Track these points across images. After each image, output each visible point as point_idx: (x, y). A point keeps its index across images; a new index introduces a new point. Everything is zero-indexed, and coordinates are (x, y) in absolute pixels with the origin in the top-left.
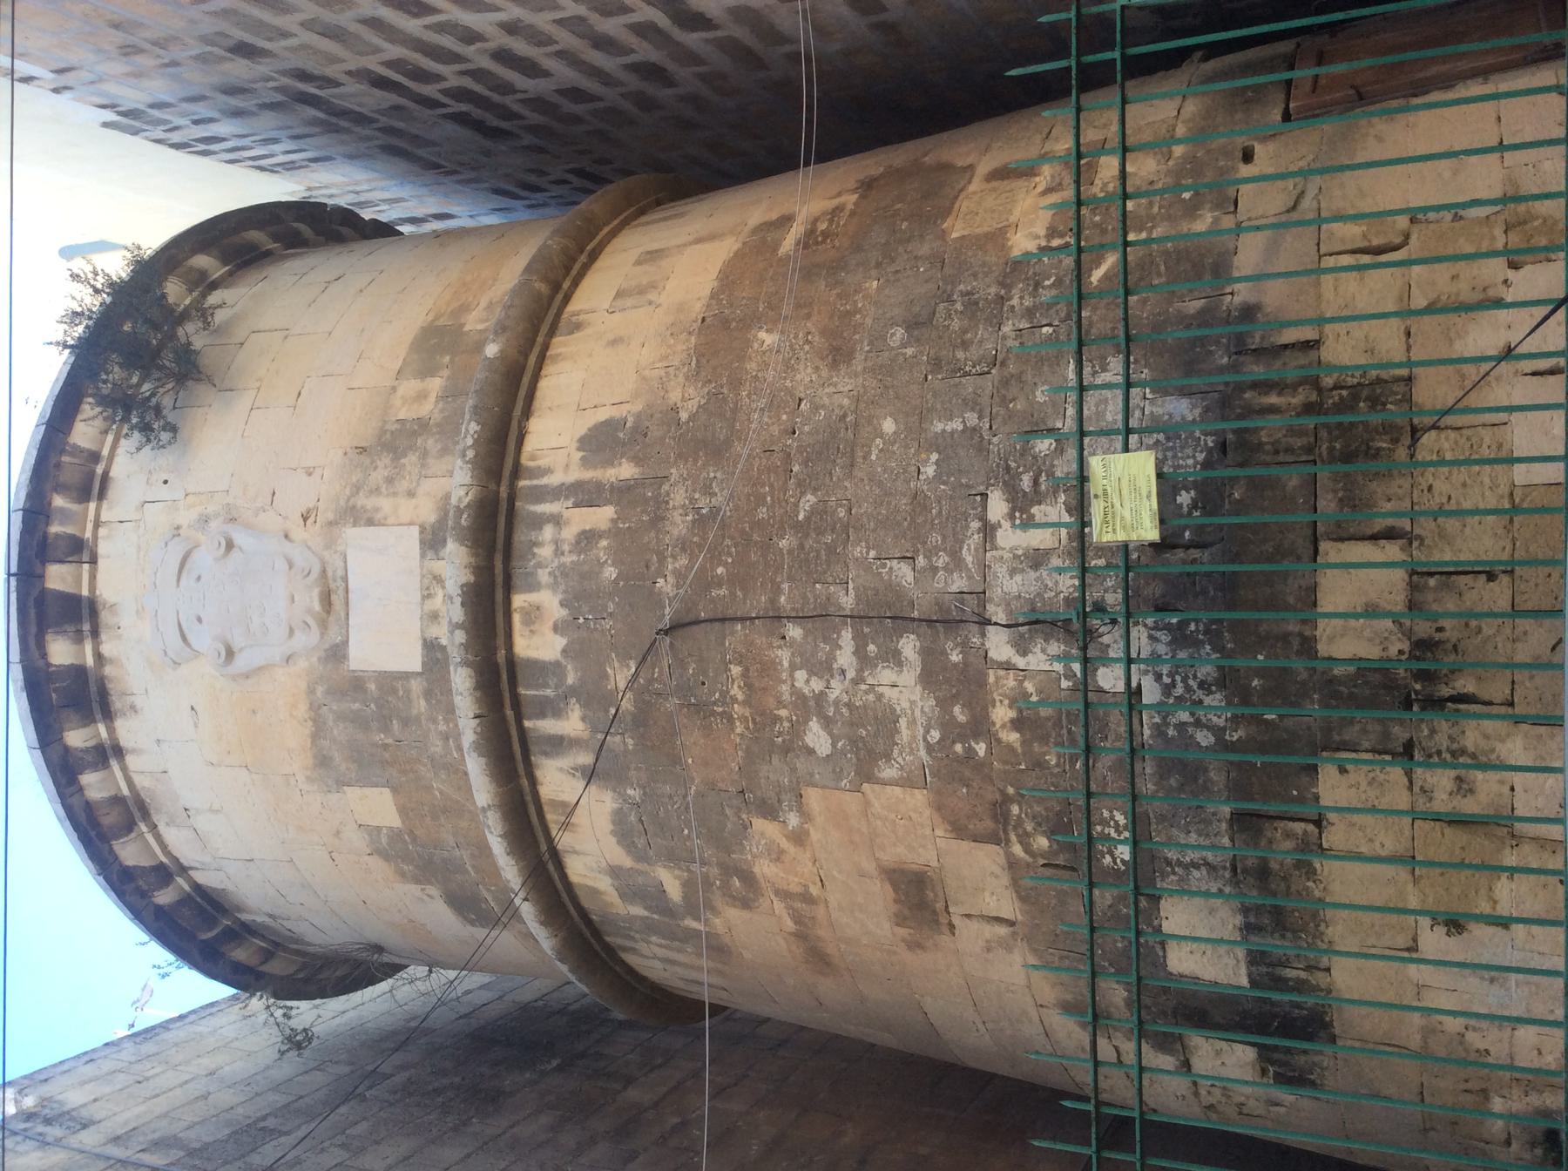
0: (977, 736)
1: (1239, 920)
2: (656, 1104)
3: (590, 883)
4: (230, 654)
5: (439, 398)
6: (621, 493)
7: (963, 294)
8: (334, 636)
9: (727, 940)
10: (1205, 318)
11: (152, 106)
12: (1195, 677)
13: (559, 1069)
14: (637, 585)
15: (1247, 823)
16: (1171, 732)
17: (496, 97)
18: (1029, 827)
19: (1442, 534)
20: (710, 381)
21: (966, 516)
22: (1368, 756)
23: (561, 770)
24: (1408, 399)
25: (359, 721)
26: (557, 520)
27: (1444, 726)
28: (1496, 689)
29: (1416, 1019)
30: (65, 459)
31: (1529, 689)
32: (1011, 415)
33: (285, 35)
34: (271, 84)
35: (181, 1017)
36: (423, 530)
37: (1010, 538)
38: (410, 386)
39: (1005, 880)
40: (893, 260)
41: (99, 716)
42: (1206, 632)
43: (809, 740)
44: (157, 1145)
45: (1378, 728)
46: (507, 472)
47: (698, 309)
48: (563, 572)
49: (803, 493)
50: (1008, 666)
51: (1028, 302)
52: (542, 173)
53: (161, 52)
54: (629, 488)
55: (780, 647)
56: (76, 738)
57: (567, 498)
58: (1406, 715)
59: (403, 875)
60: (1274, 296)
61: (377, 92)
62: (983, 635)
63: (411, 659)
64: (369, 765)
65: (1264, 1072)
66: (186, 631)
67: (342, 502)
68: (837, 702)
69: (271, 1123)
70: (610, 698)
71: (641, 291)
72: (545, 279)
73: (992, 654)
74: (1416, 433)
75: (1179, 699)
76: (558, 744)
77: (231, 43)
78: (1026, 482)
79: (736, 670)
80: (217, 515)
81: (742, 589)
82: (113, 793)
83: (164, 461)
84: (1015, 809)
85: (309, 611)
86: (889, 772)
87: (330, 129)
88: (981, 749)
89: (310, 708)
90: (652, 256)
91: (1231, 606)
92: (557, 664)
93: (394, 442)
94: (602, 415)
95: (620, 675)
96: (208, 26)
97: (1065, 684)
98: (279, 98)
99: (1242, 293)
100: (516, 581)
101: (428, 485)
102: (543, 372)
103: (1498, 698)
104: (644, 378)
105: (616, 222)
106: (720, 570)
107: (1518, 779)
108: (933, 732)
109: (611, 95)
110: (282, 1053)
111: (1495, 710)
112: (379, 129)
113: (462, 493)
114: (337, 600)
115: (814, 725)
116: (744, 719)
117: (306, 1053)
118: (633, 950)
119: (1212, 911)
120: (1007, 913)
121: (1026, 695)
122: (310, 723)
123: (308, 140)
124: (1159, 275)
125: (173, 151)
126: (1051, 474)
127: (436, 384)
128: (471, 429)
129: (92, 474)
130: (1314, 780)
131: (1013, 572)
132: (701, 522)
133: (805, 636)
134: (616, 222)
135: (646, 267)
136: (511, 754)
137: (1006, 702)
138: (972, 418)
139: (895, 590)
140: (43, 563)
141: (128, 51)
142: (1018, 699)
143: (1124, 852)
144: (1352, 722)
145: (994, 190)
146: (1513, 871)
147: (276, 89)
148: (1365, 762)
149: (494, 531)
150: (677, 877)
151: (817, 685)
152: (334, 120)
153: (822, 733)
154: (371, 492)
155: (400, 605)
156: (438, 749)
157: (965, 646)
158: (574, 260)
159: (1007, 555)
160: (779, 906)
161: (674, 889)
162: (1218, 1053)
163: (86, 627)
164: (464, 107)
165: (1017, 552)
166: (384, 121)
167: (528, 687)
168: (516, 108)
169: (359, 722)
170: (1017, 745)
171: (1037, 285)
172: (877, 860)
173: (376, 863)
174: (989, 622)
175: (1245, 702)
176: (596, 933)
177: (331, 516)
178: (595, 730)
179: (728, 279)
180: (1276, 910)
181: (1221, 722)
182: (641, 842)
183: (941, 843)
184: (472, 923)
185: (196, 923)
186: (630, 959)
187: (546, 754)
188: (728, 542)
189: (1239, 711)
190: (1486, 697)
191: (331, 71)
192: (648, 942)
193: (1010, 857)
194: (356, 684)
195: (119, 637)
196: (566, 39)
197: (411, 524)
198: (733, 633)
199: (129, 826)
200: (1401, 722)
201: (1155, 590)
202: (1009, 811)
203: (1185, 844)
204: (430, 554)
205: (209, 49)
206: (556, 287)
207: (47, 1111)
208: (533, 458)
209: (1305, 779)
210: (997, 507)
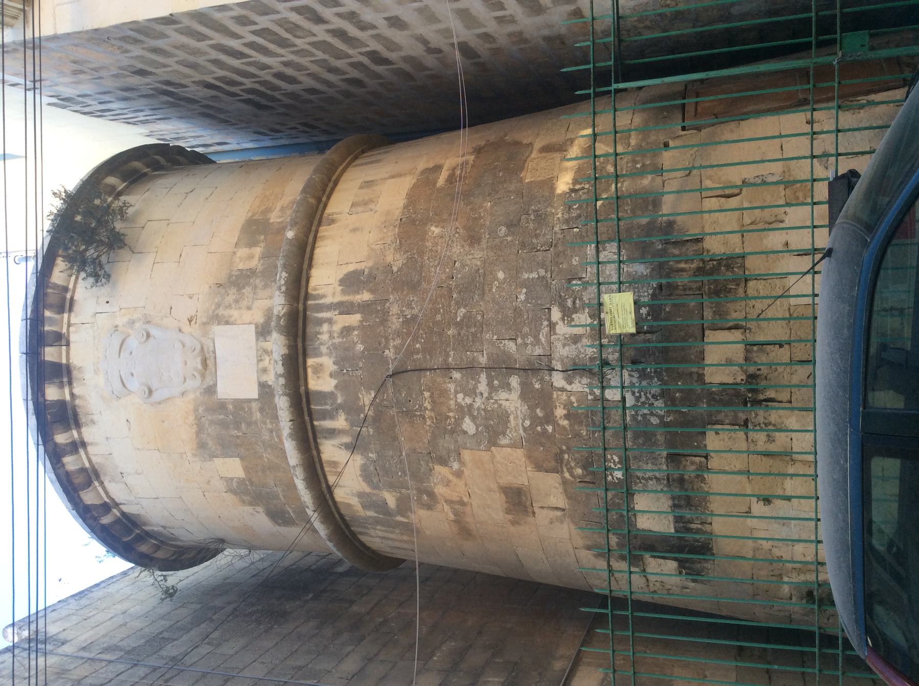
0: (548, 423)
1: (670, 503)
2: (368, 613)
3: (346, 501)
4: (151, 392)
6: (363, 308)
7: (534, 211)
8: (209, 381)
10: (650, 229)
11: (79, 96)
14: (374, 354)
15: (673, 458)
16: (639, 418)
17: (269, 92)
18: (573, 464)
19: (759, 327)
22: (728, 427)
23: (334, 445)
24: (743, 267)
25: (224, 424)
26: (330, 321)
27: (761, 413)
28: (784, 396)
29: (750, 543)
30: (49, 291)
31: (799, 396)
32: (560, 271)
35: (97, 585)
37: (562, 329)
38: (243, 252)
39: (561, 490)
40: (497, 192)
41: (73, 426)
42: (655, 372)
44: (107, 650)
45: (733, 414)
47: (397, 214)
48: (335, 347)
49: (459, 308)
50: (563, 390)
54: (368, 305)
56: (61, 438)
57: (335, 310)
58: (746, 409)
59: (243, 502)
61: (206, 90)
62: (551, 375)
63: (253, 392)
64: (227, 448)
65: (680, 573)
66: (125, 382)
67: (211, 312)
68: (478, 409)
69: (166, 635)
70: (361, 409)
71: (366, 203)
72: (314, 197)
73: (556, 384)
74: (746, 280)
75: (643, 403)
76: (332, 433)
77: (135, 69)
78: (569, 303)
79: (427, 394)
80: (139, 320)
82: (80, 466)
83: (104, 291)
84: (566, 456)
85: (196, 369)
86: (504, 441)
87: (172, 105)
88: (550, 429)
89: (196, 419)
90: (368, 184)
91: (666, 361)
92: (332, 393)
93: (237, 282)
94: (351, 268)
95: (366, 398)
96: (126, 62)
97: (590, 397)
98: (152, 92)
100: (309, 352)
101: (258, 303)
103: (785, 399)
104: (372, 249)
105: (344, 164)
106: (418, 346)
107: (794, 435)
109: (331, 92)
110: (163, 600)
111: (783, 405)
114: (210, 363)
115: (467, 420)
117: (174, 598)
118: (366, 534)
119: (658, 499)
120: (561, 505)
123: (160, 111)
124: (628, 204)
126: (581, 299)
127: (258, 251)
128: (282, 276)
129: (64, 298)
130: (705, 439)
131: (564, 346)
132: (407, 322)
133: (462, 378)
134: (347, 161)
135: (365, 191)
136: (308, 438)
138: (542, 272)
139: (508, 356)
141: (75, 73)
142: (568, 405)
143: (619, 474)
144: (721, 412)
145: (545, 158)
146: (792, 476)
147: (151, 89)
148: (728, 430)
149: (298, 327)
151: (468, 400)
153: (472, 424)
154: (227, 307)
155: (245, 363)
156: (267, 437)
157: (542, 380)
159: (561, 338)
160: (447, 508)
162: (660, 565)
163: (65, 380)
164: (250, 96)
165: (566, 337)
166: (206, 102)
167: (316, 405)
168: (279, 97)
169: (223, 425)
170: (567, 426)
171: (570, 207)
172: (498, 483)
174: (554, 370)
175: (674, 405)
176: (348, 526)
177: (205, 320)
178: (352, 425)
179: (412, 199)
180: (687, 497)
181: (662, 413)
183: (530, 474)
184: (279, 525)
185: (122, 532)
186: (363, 538)
187: (326, 438)
189: (670, 408)
190: (780, 399)
191: (183, 82)
192: (375, 529)
193: (563, 478)
194: (222, 406)
195: (84, 384)
196: (315, 68)
197: (250, 323)
199: (89, 483)
200: (743, 412)
201: (631, 353)
203: (646, 469)
204: (261, 339)
206: (319, 200)
208: (315, 289)
209: (700, 438)
210: (556, 314)
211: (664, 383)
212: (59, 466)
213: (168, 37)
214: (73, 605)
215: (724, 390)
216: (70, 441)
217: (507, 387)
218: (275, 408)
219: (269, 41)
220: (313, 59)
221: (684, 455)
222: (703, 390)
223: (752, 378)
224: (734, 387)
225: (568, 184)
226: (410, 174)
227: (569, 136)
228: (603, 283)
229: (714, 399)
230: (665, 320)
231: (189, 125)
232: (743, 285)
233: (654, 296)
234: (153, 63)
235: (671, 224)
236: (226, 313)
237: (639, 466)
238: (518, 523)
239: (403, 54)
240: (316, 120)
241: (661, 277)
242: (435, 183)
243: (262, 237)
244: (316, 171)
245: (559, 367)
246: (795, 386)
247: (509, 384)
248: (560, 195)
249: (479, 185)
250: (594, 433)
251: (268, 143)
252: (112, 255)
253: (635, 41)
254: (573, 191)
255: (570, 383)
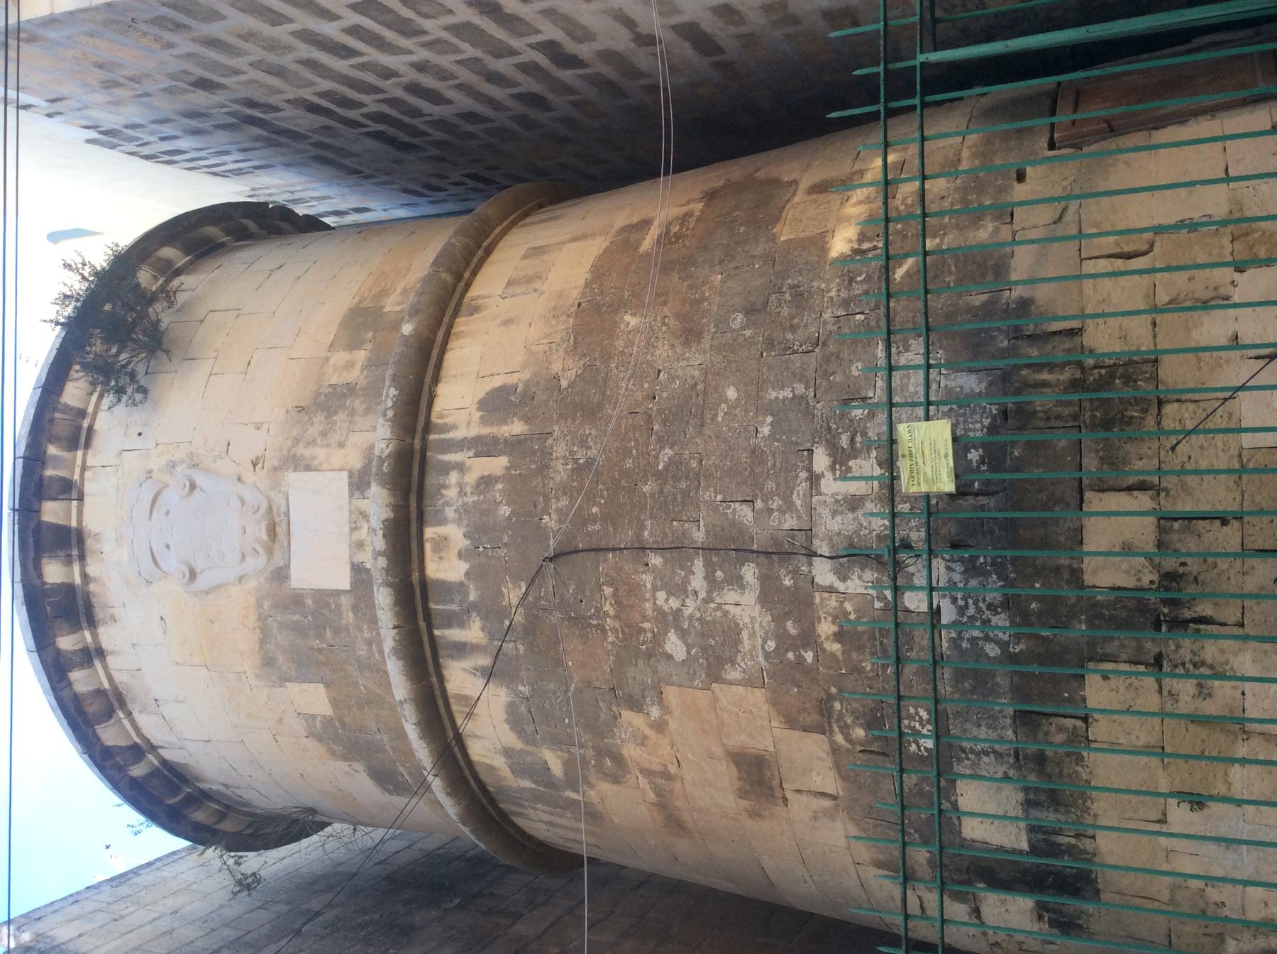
0: (805, 646)
1: (1020, 796)
3: (487, 761)
4: (193, 574)
5: (364, 367)
6: (513, 446)
7: (791, 287)
9: (600, 808)
10: (988, 311)
11: (127, 127)
12: (984, 600)
13: (460, 907)
15: (1027, 720)
16: (965, 645)
17: (406, 119)
18: (849, 720)
19: (1184, 487)
20: (585, 355)
21: (795, 467)
23: (464, 670)
24: (1155, 378)
25: (299, 630)
26: (461, 467)
27: (1187, 643)
28: (1230, 613)
30: (57, 415)
32: (831, 386)
33: (237, 72)
34: (225, 110)
35: (149, 864)
36: (351, 475)
37: (831, 486)
38: (340, 357)
39: (829, 763)
40: (733, 258)
41: (85, 625)
42: (993, 564)
43: (669, 647)
45: (1134, 644)
46: (420, 428)
47: (575, 295)
48: (466, 510)
49: (662, 448)
50: (831, 590)
51: (844, 294)
52: (442, 177)
53: (137, 86)
54: (519, 442)
55: (644, 572)
56: (67, 643)
57: (469, 449)
59: (333, 753)
60: (1042, 293)
61: (310, 115)
62: (810, 564)
63: (343, 581)
64: (306, 665)
67: (285, 452)
68: (691, 617)
70: (504, 612)
71: (528, 280)
72: (449, 270)
74: (1161, 403)
76: (462, 649)
77: (193, 79)
78: (844, 441)
79: (608, 591)
81: (613, 525)
83: (138, 415)
84: (837, 706)
85: (258, 540)
86: (734, 674)
87: (270, 143)
88: (809, 656)
89: (259, 619)
90: (537, 251)
91: (1013, 545)
92: (461, 584)
93: (327, 403)
94: (497, 382)
95: (513, 594)
96: (175, 66)
97: (878, 605)
98: (232, 120)
99: (1017, 292)
100: (427, 517)
102: (449, 347)
103: (1232, 620)
104: (531, 352)
106: (595, 510)
107: (1248, 686)
108: (769, 642)
110: (235, 894)
112: (312, 144)
113: (384, 446)
114: (281, 530)
115: (672, 636)
116: (614, 630)
120: (831, 789)
121: (847, 614)
122: (258, 631)
123: (256, 153)
124: (950, 273)
125: (144, 161)
126: (864, 434)
127: (361, 355)
129: (79, 428)
130: (1082, 686)
131: (834, 514)
132: (579, 470)
133: (665, 564)
134: (505, 223)
136: (424, 657)
137: (830, 619)
138: (800, 388)
139: (738, 528)
140: (40, 501)
141: (109, 85)
142: (839, 616)
144: (1112, 639)
145: (815, 201)
147: (227, 113)
149: (409, 477)
150: (559, 758)
151: (674, 603)
152: (275, 137)
153: (679, 642)
154: (309, 443)
155: (333, 534)
157: (795, 573)
158: (473, 254)
159: (829, 500)
160: (643, 781)
161: (556, 766)
163: (75, 552)
164: (381, 127)
165: (838, 498)
166: (316, 138)
167: (437, 603)
168: (423, 127)
169: (299, 629)
170: (839, 654)
171: (851, 280)
173: (312, 745)
174: (815, 555)
176: (493, 802)
178: (492, 638)
179: (599, 272)
180: (1050, 785)
181: (1005, 637)
182: (529, 729)
183: (777, 732)
184: (391, 793)
185: (162, 790)
186: (519, 821)
187: (452, 657)
188: (601, 486)
190: (1222, 620)
191: (272, 100)
192: (535, 809)
193: (832, 742)
194: (296, 600)
195: (102, 560)
196: (465, 75)
197: (341, 470)
198: (605, 561)
199: (109, 714)
202: (832, 706)
204: (357, 494)
205: (175, 83)
206: (458, 277)
207: (41, 945)
208: (441, 416)
210: (821, 460)
211: (1010, 584)
212: (64, 684)
213: (224, 18)
214: (107, 894)
215: (1118, 600)
216: (80, 646)
217: (737, 582)
218: (372, 606)
219: (379, 22)
220: (459, 57)
221: (1044, 714)
222: (1079, 599)
223: (1171, 579)
224: (1138, 594)
225: (851, 241)
226: (601, 233)
227: (857, 167)
228: (897, 405)
229: (1101, 616)
230: (1012, 471)
231: (304, 179)
232: (1154, 411)
233: (992, 429)
234: (215, 66)
235: (1024, 305)
236: (308, 452)
237: (965, 731)
238: (760, 815)
239: (596, 46)
240: (489, 168)
241: (1005, 394)
242: (637, 248)
243: (371, 334)
244: (455, 234)
245: (824, 550)
246: (1250, 596)
247: (741, 578)
248: (836, 260)
249: (705, 248)
250: (885, 667)
251: (428, 209)
252: (152, 363)
253: (978, 18)
254: (857, 252)
255: (844, 579)
